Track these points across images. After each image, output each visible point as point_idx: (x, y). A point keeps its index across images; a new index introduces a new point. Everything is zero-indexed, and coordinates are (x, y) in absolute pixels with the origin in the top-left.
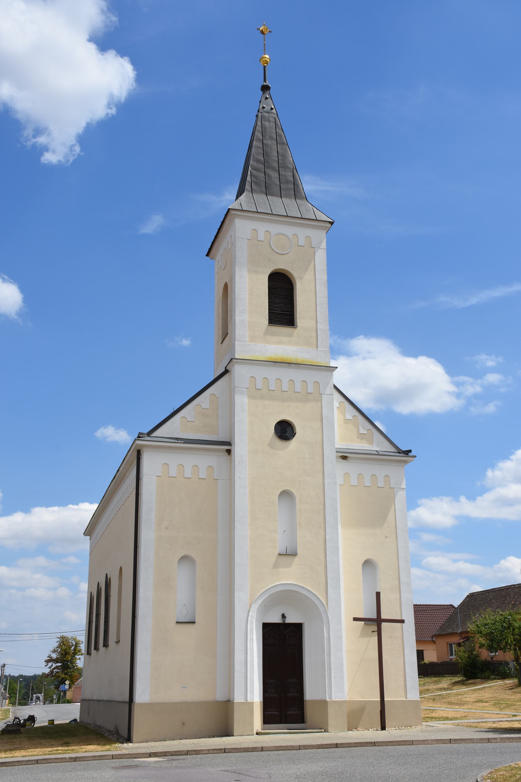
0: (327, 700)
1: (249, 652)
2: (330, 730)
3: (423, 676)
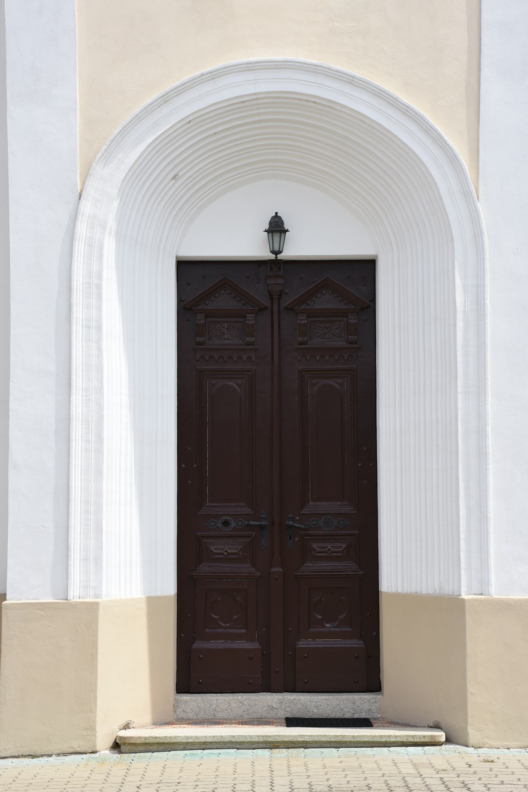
0: (464, 596)
1: (78, 381)
2: (473, 736)
3: (244, 504)
